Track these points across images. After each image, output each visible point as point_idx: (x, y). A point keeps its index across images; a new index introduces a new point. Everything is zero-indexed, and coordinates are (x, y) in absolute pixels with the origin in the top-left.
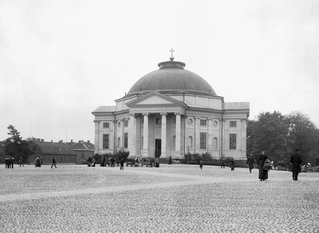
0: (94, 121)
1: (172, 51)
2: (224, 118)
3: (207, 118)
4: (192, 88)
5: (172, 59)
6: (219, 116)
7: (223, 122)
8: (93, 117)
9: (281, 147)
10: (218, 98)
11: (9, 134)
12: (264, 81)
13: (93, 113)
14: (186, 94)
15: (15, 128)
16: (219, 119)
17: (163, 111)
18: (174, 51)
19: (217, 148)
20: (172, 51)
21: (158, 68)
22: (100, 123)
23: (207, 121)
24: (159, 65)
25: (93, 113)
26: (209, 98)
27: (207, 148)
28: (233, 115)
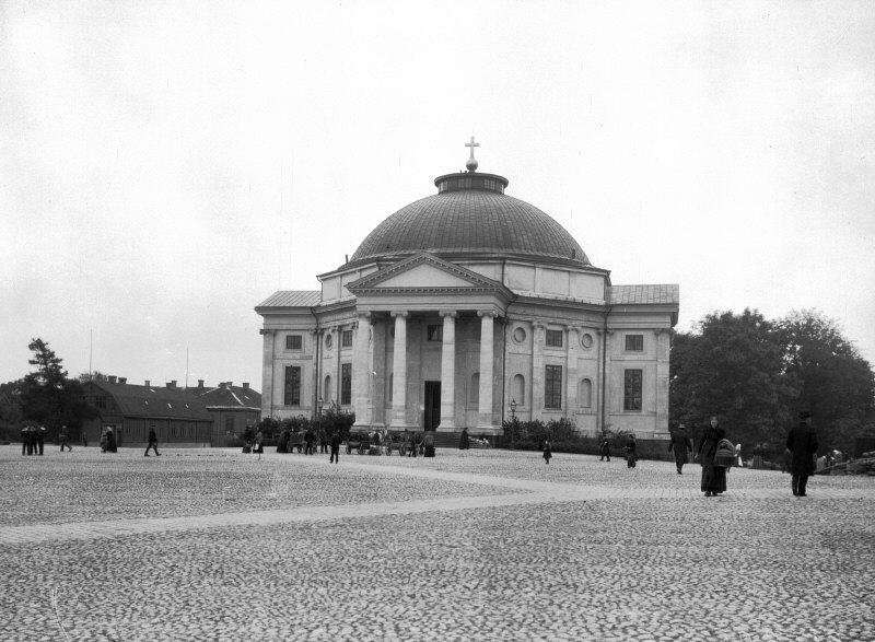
0: (262, 332)
1: (473, 145)
2: (610, 326)
3: (565, 326)
5: (472, 167)
6: (597, 322)
8: (259, 321)
13: (258, 309)
15: (51, 347)
16: (598, 329)
20: (473, 145)
25: (258, 309)
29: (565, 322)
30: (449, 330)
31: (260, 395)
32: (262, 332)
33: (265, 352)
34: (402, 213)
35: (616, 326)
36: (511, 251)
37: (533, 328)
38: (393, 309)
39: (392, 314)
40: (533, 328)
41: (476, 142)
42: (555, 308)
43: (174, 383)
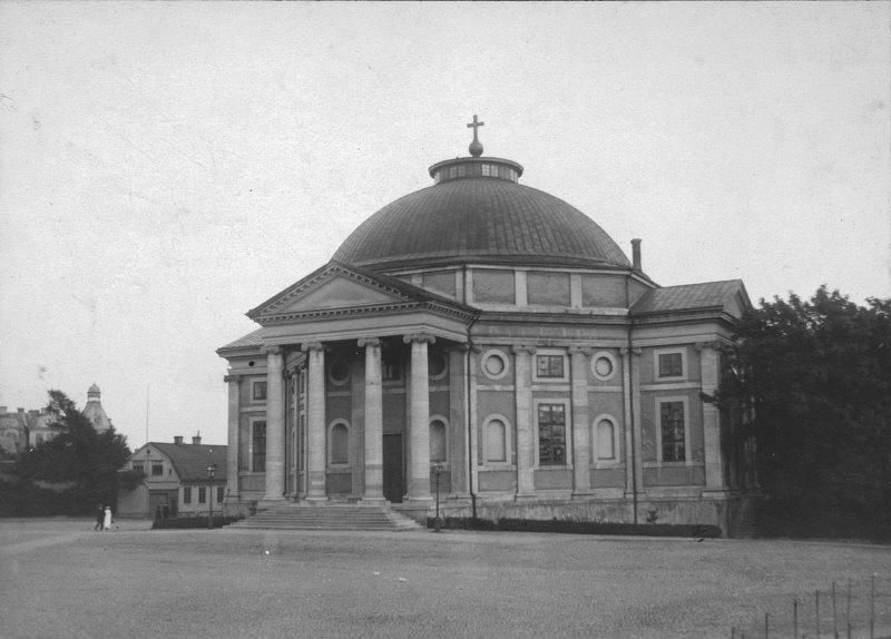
0: (227, 379)
1: (476, 124)
2: (636, 343)
3: (567, 348)
4: (522, 236)
5: (476, 149)
6: (619, 338)
7: (635, 359)
8: (224, 366)
9: (845, 411)
10: (608, 272)
11: (869, 301)
12: (758, 191)
13: (222, 352)
14: (471, 266)
15: (103, 399)
16: (618, 349)
17: (364, 330)
18: (482, 124)
19: (613, 458)
20: (476, 124)
21: (431, 182)
22: (243, 386)
23: (566, 361)
24: (433, 172)
25: (222, 352)
26: (569, 274)
27: (569, 460)
28: (667, 332)
29: (566, 343)
30: (373, 365)
31: (130, 454)
32: (227, 379)
33: (230, 405)
34: (359, 233)
35: (646, 343)
36: (485, 252)
37: (513, 354)
38: (305, 341)
39: (406, 340)
40: (513, 354)
41: (479, 121)
42: (523, 323)
43: (182, 438)
